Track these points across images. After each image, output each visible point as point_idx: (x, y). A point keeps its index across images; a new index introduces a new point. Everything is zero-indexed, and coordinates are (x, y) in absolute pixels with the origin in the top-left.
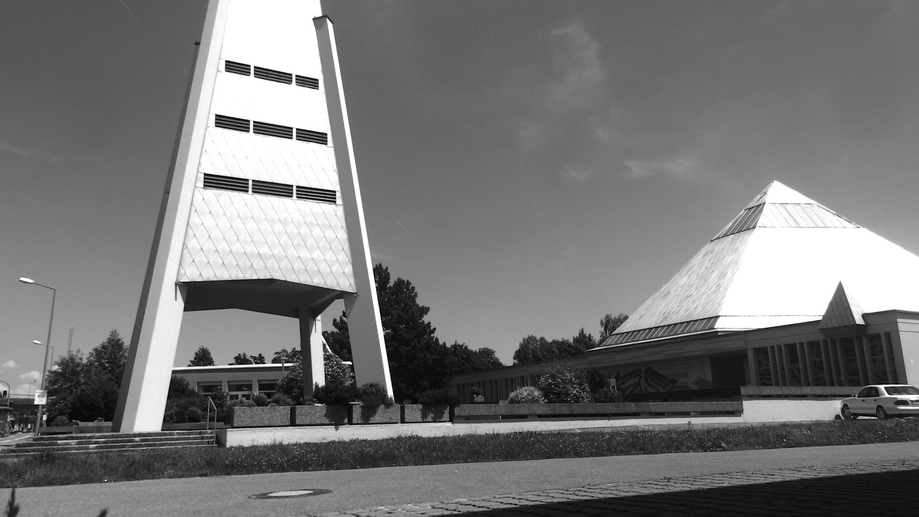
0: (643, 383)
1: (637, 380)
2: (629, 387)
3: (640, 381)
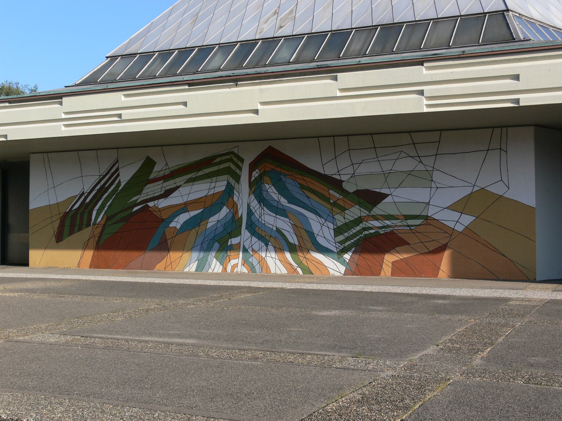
0: (244, 198)
1: (220, 185)
2: (184, 207)
3: (229, 191)
